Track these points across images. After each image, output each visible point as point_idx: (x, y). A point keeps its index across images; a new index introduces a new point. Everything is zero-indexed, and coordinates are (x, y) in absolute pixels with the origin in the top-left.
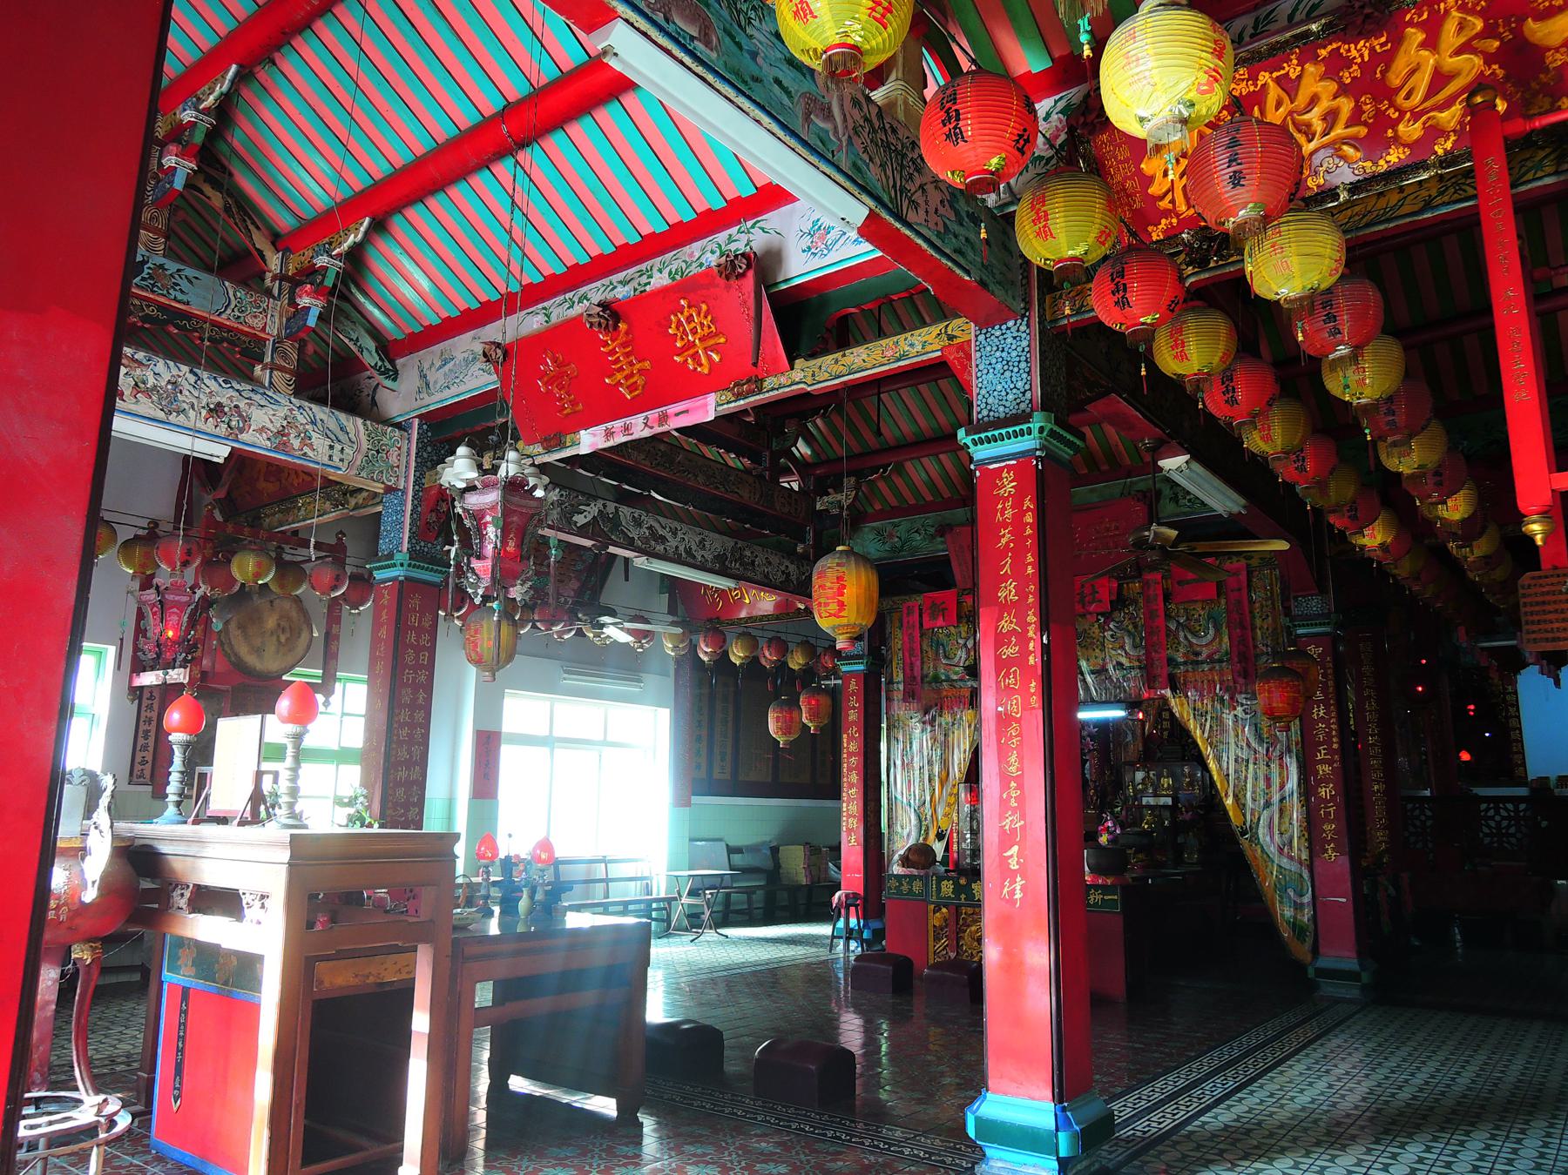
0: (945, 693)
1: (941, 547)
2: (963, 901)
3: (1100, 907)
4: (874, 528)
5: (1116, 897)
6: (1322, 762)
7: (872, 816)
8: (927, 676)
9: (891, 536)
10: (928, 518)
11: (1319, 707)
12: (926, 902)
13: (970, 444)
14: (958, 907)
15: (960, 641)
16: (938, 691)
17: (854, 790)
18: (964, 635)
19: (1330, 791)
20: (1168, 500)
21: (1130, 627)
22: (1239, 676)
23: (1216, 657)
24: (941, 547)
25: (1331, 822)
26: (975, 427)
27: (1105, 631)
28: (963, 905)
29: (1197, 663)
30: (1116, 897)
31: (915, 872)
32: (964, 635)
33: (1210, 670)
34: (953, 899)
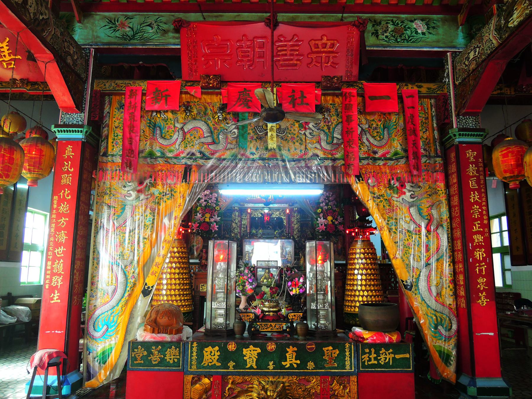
0: (160, 168)
1: (172, 41)
2: (231, 370)
3: (392, 367)
4: (105, 17)
5: (407, 356)
6: (477, 233)
7: (77, 274)
8: (142, 152)
9: (123, 25)
10: (162, 16)
11: (474, 193)
12: (183, 373)
13: (56, 131)
14: (223, 378)
15: (177, 125)
16: (153, 166)
17: (61, 249)
18: (181, 120)
19: (483, 255)
20: (371, 34)
21: (325, 128)
22: (414, 168)
23: (388, 156)
24: (172, 41)
25: (483, 277)
26: (57, 126)
27: (306, 129)
28: (232, 374)
29: (375, 159)
30: (407, 356)
31: (168, 338)
32: (181, 120)
33: (384, 165)
34: (218, 368)
